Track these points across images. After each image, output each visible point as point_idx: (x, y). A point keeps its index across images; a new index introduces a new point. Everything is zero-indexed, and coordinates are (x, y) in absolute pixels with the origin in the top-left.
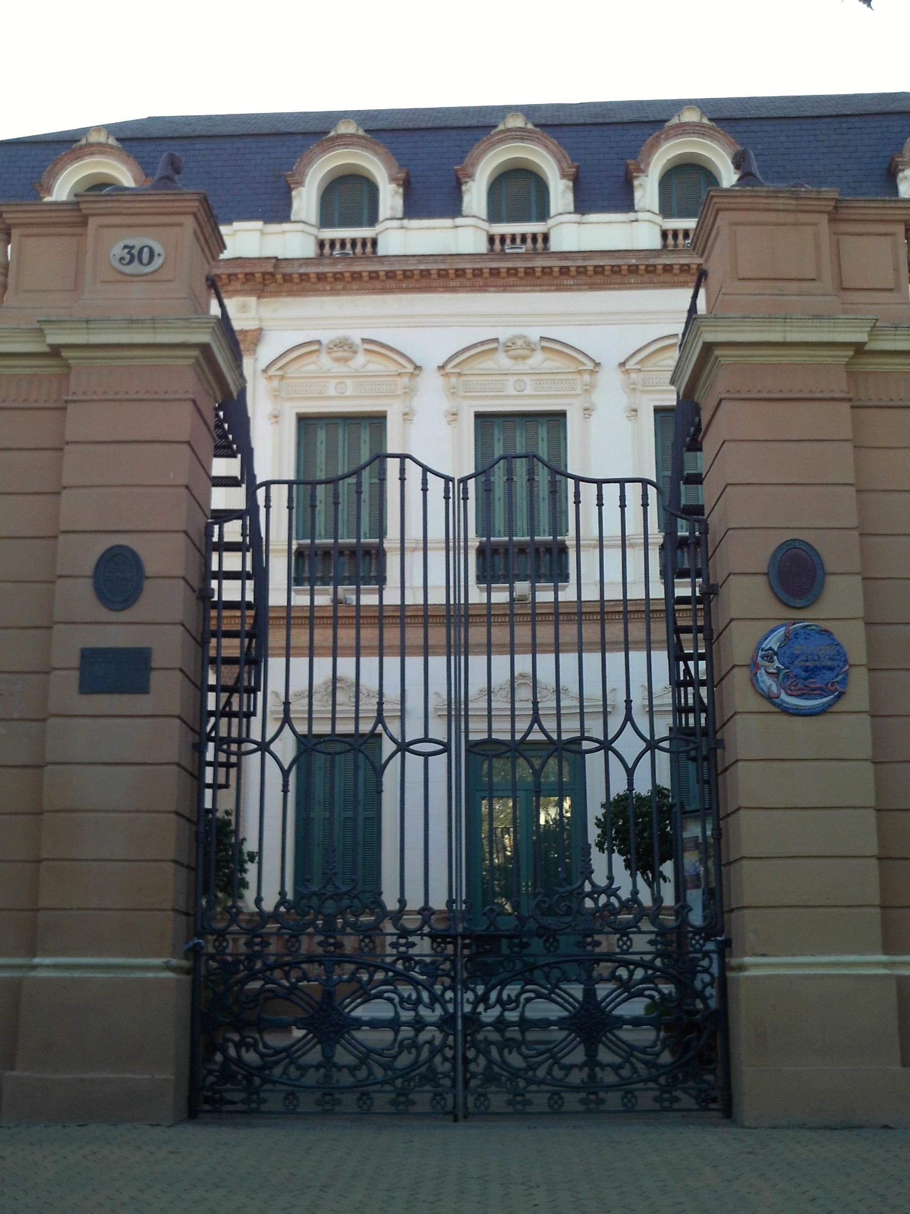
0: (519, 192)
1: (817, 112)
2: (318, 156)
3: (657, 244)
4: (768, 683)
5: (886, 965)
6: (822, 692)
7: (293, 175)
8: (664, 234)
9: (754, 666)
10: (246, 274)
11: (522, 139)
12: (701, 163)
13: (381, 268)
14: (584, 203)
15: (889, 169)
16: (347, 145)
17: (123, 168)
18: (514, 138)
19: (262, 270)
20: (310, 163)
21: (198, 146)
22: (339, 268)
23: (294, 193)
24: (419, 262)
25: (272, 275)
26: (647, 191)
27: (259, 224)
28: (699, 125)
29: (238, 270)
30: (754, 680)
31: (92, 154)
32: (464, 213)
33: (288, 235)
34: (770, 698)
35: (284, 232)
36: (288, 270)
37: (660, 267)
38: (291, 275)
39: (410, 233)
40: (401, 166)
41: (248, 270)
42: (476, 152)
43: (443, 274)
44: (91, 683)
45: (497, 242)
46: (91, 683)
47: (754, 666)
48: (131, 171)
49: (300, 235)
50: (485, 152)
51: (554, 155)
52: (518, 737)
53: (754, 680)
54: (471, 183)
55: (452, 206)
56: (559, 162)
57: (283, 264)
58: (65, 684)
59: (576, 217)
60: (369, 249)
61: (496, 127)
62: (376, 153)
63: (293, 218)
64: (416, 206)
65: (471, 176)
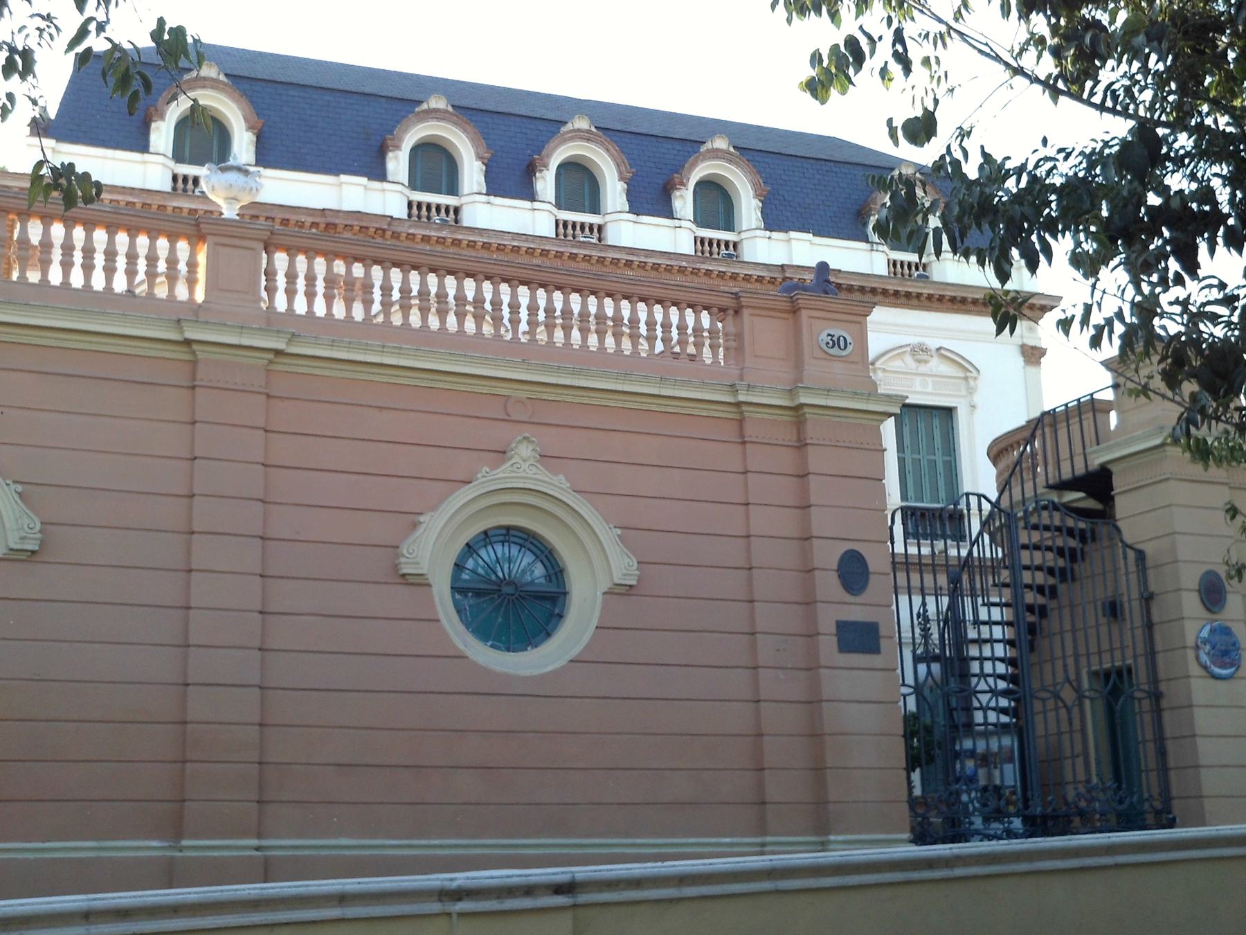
0: (435, 167)
1: (761, 146)
2: (414, 124)
3: (167, 187)
4: (1205, 658)
5: (257, 849)
6: (1232, 665)
7: (393, 139)
8: (175, 178)
9: (1197, 648)
10: (328, 225)
11: (588, 140)
12: (451, 151)
13: (743, 271)
14: (497, 185)
15: (528, 166)
16: (438, 119)
17: (234, 106)
18: (582, 138)
19: (377, 226)
20: (406, 131)
21: (327, 98)
22: (444, 234)
23: (153, 125)
24: (513, 240)
25: (384, 230)
26: (398, 163)
27: (364, 180)
28: (446, 112)
29: (356, 223)
30: (1197, 658)
31: (204, 87)
32: (390, 178)
33: (149, 166)
34: (1205, 668)
35: (144, 162)
36: (399, 229)
37: (186, 211)
38: (399, 234)
39: (496, 209)
40: (489, 147)
41: (364, 224)
42: (552, 144)
43: (953, 300)
44: (846, 646)
45: (180, 181)
46: (846, 646)
47: (1197, 648)
48: (242, 110)
49: (160, 167)
50: (557, 147)
51: (614, 159)
52: (911, 690)
53: (1197, 658)
54: (545, 172)
55: (141, 144)
56: (618, 165)
57: (395, 223)
58: (828, 644)
59: (632, 217)
60: (190, 185)
61: (420, 102)
62: (465, 131)
63: (151, 150)
64: (497, 185)
65: (162, 117)
